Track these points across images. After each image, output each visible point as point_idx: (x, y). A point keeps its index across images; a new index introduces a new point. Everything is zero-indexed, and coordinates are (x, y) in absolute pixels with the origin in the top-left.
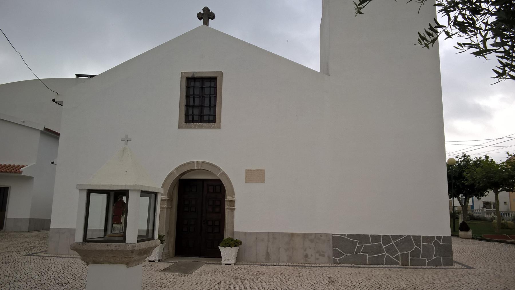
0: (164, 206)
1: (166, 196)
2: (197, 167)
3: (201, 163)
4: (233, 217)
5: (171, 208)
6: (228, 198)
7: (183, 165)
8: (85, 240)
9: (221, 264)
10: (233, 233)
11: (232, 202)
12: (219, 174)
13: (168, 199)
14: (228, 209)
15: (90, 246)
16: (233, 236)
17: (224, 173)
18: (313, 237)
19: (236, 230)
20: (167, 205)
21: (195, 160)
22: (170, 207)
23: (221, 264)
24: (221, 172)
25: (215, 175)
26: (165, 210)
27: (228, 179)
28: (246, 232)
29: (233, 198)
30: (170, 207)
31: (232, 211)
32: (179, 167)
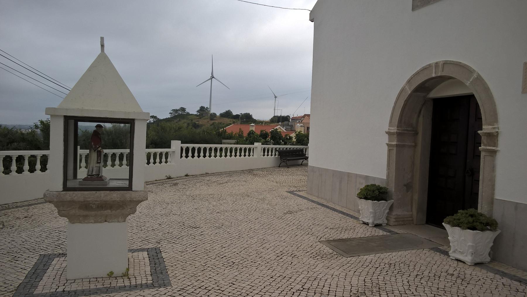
0: (393, 143)
1: (396, 128)
2: (435, 73)
3: (442, 64)
4: (493, 169)
5: (415, 146)
6: (486, 128)
7: (418, 73)
8: (66, 188)
9: (446, 253)
10: (492, 201)
11: (493, 137)
12: (471, 80)
13: (400, 131)
14: (485, 151)
15: (70, 196)
16: (492, 207)
17: (479, 79)
18: (492, 252)
19: (498, 196)
20: (398, 141)
21: (433, 61)
22: (413, 144)
23: (446, 253)
24: (475, 76)
25: (461, 84)
26: (395, 149)
27: (487, 89)
28: (517, 203)
29: (494, 128)
30: (413, 144)
31: (493, 156)
32: (411, 78)
